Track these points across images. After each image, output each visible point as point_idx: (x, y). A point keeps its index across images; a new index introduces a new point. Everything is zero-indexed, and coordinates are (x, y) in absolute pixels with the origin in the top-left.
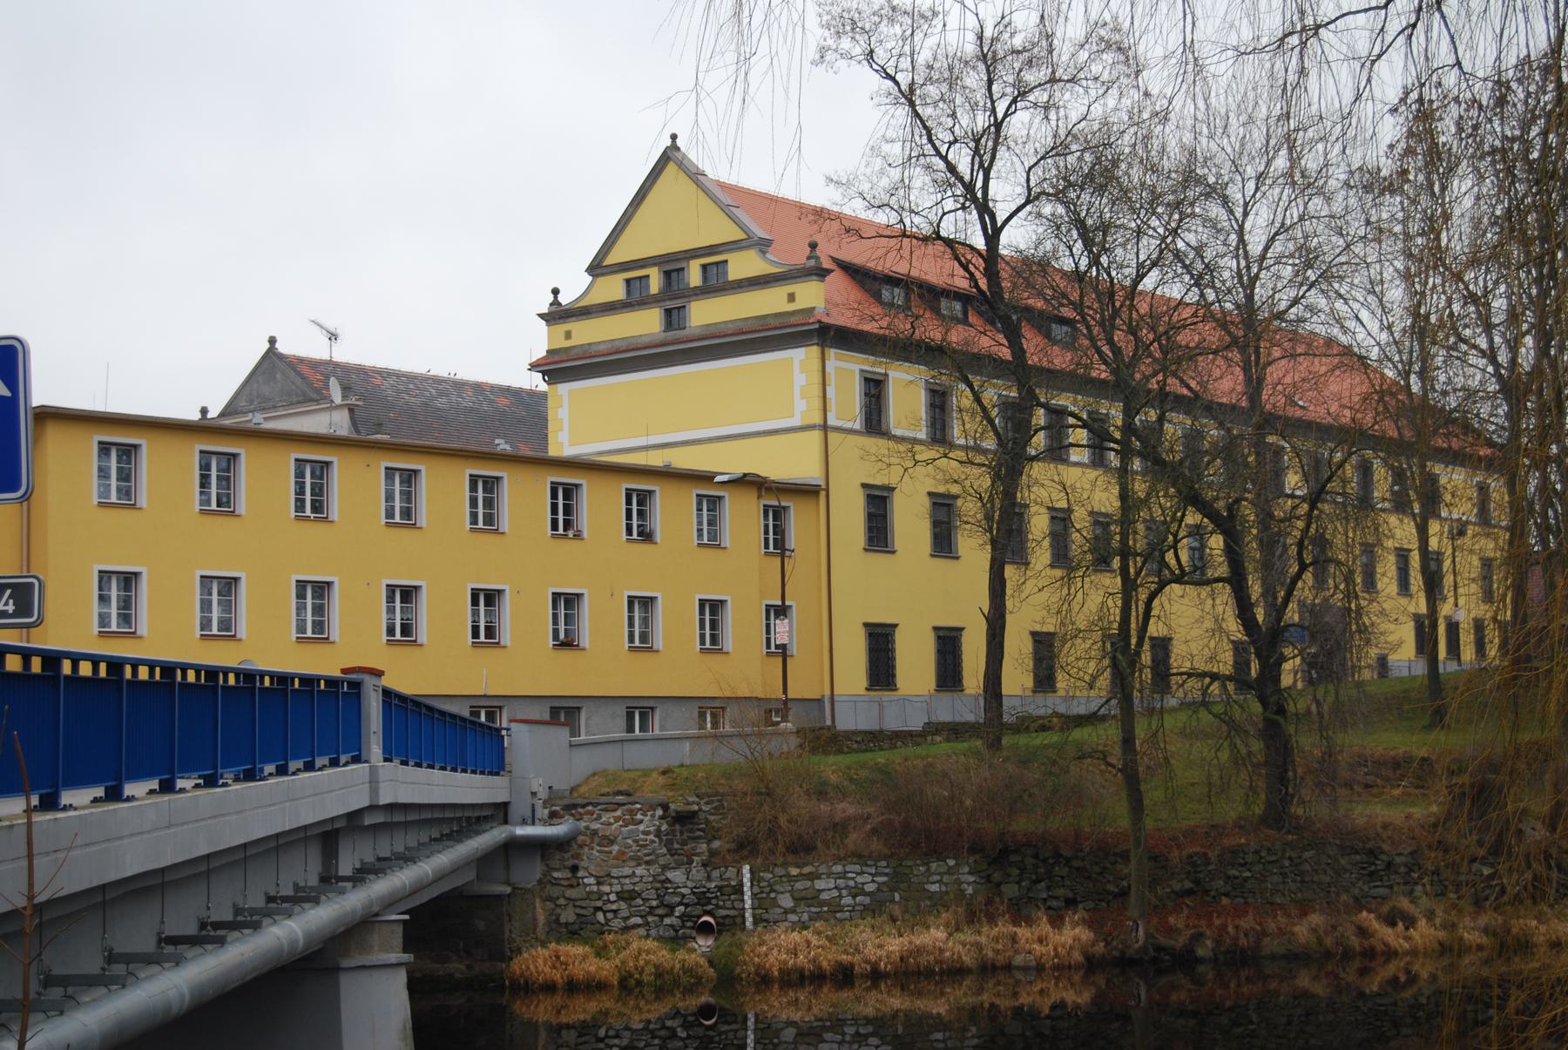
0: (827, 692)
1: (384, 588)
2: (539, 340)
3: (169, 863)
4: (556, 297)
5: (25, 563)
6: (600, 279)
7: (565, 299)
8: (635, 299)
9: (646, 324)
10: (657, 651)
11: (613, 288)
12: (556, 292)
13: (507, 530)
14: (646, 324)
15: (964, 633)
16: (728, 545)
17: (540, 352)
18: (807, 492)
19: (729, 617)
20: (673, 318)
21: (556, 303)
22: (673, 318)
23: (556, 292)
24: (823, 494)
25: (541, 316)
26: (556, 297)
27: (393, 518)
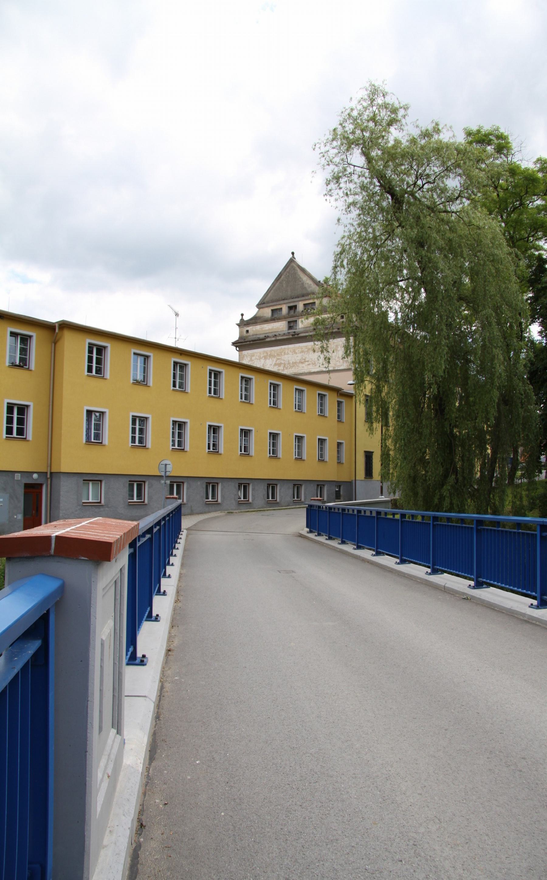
0: (354, 479)
1: (131, 418)
2: (235, 335)
3: (89, 712)
4: (242, 317)
5: (51, 404)
6: (261, 310)
7: (246, 318)
8: (275, 316)
9: (281, 326)
10: (304, 460)
11: (267, 312)
12: (242, 315)
13: (254, 403)
14: (281, 326)
15: (374, 454)
16: (328, 416)
17: (236, 338)
18: (349, 396)
19: (281, 440)
20: (292, 325)
21: (242, 320)
22: (292, 325)
23: (242, 315)
24: (354, 397)
25: (238, 325)
26: (242, 317)
27: (12, 434)
